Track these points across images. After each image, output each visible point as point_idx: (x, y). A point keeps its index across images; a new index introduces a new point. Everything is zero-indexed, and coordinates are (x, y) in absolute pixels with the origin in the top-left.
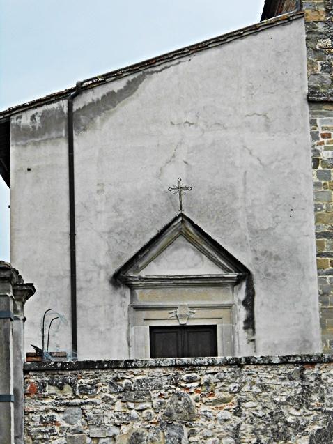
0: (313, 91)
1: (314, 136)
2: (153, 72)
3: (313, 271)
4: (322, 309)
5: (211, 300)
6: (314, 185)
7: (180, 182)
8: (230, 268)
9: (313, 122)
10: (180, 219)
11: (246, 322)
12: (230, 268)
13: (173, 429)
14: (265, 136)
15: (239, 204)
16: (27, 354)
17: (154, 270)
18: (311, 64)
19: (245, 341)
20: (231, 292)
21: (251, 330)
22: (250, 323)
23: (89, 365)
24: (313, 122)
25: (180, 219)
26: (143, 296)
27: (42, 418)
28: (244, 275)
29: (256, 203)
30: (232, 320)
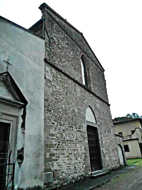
2: (2, 21)
3: (43, 111)
4: (44, 125)
5: (10, 112)
6: (35, 175)
7: (8, 61)
8: (19, 100)
10: (6, 74)
11: (22, 124)
12: (19, 100)
15: (24, 80)
19: (21, 133)
20: (18, 111)
21: (23, 128)
22: (23, 125)
25: (6, 74)
29: (29, 82)
30: (17, 123)
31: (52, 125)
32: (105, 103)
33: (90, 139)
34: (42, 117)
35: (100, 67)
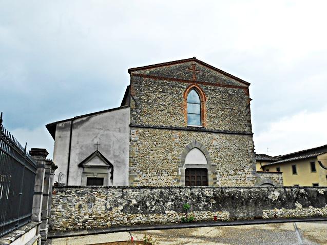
0: (131, 124)
1: (130, 134)
3: (128, 166)
9: (130, 131)
17: (90, 164)
18: (131, 118)
22: (112, 178)
24: (130, 131)
26: (86, 170)
27: (161, 193)
28: (111, 166)
30: (107, 177)
31: (136, 174)
32: (236, 135)
33: (188, 180)
34: (128, 170)
35: (238, 83)
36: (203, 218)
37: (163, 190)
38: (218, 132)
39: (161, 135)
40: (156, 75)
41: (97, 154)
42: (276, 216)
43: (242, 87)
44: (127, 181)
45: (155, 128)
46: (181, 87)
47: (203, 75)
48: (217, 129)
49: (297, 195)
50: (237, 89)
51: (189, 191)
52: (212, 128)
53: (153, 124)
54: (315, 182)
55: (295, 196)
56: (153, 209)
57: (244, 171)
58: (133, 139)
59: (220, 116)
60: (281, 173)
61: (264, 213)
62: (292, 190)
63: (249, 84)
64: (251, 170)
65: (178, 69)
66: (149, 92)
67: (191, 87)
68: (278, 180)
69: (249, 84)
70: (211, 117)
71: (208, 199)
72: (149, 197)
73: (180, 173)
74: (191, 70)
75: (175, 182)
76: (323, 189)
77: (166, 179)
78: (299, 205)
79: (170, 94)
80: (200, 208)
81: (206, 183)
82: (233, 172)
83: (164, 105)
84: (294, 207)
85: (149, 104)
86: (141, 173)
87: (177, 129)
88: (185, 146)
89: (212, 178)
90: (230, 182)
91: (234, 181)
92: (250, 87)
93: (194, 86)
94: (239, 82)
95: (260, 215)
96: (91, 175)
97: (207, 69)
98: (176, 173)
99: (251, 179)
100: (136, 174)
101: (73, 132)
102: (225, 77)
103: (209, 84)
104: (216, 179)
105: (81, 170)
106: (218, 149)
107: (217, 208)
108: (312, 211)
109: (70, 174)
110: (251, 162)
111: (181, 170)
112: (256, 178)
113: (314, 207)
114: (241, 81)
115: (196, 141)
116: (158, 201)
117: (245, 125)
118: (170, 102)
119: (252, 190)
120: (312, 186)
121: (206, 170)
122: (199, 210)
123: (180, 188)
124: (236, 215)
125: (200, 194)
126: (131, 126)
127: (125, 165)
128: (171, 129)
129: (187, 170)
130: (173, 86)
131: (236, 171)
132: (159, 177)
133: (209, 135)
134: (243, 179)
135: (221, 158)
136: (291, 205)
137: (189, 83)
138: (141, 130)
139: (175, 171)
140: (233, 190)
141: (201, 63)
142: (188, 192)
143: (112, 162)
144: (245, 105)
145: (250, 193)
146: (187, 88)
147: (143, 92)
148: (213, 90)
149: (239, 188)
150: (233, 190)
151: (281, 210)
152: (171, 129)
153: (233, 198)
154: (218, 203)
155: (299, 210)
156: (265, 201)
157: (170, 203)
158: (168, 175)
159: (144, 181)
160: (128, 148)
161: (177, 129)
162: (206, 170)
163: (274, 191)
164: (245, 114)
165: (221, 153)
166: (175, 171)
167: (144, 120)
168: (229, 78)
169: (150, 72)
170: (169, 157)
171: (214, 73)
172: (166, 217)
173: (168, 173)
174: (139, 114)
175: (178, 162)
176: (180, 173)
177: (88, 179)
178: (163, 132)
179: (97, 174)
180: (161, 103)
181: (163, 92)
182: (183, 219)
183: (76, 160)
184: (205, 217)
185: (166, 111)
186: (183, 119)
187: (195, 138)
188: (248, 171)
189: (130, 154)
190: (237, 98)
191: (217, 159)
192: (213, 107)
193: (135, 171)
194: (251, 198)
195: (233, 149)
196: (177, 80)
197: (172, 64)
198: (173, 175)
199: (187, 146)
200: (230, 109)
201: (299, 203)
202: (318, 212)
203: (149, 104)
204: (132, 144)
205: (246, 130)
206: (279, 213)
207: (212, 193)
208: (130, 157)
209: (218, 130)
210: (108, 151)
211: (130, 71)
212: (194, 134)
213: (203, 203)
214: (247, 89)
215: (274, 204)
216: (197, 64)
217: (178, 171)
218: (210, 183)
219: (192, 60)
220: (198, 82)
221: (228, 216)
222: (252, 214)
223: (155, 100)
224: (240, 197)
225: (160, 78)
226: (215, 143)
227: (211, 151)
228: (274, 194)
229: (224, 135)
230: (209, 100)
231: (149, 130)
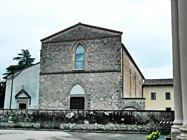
0: (41, 72)
1: (40, 79)
3: (38, 97)
9: (40, 77)
13: (87, 113)
14: (34, 79)
16: (155, 93)
17: (20, 96)
18: (41, 69)
22: (30, 104)
23: (125, 98)
24: (40, 77)
26: (19, 100)
27: (7, 112)
28: (29, 97)
31: (42, 101)
32: (107, 73)
33: (72, 105)
36: (26, 126)
37: (8, 111)
38: (94, 72)
39: (56, 78)
40: (55, 41)
41: (23, 91)
42: (69, 128)
43: (116, 36)
44: (37, 105)
45: (53, 73)
46: (70, 45)
47: (86, 33)
48: (93, 70)
49: (87, 115)
50: (111, 39)
51: (21, 112)
52: (90, 69)
53: (52, 71)
54: (168, 107)
55: (85, 116)
56: (3, 120)
57: (111, 98)
58: (41, 81)
59: (96, 60)
60: (145, 99)
61: (61, 125)
62: (83, 112)
63: (122, 33)
64: (117, 97)
65: (69, 33)
66: (51, 52)
67: (77, 43)
68: (140, 104)
69: (122, 33)
70: (89, 62)
71: (29, 116)
72: (2, 114)
73: (66, 101)
74: (78, 32)
75: (63, 105)
76: (109, 112)
77: (58, 104)
78: (87, 122)
79: (63, 51)
80: (25, 120)
81: (83, 108)
82: (102, 99)
83: (60, 59)
84: (83, 123)
85: (51, 59)
86: (45, 100)
87: (66, 73)
88: (71, 83)
89: (87, 103)
90: (100, 105)
91: (103, 105)
92: (122, 36)
93: (79, 42)
94: (113, 33)
95: (58, 127)
96: (21, 102)
97: (89, 28)
98: (64, 100)
99: (117, 104)
100: (42, 101)
101: (13, 80)
102: (102, 32)
103: (89, 39)
104: (90, 103)
105: (16, 100)
106: (93, 84)
107: (34, 121)
108: (96, 126)
109: (12, 102)
110: (117, 91)
111: (67, 98)
112: (120, 102)
113: (99, 123)
114: (114, 32)
115: (78, 79)
116: (5, 116)
117: (115, 64)
118: (63, 56)
119: (56, 111)
120: (165, 110)
121: (83, 99)
122: (24, 122)
123: (16, 110)
124: (44, 126)
125: (26, 113)
126: (40, 74)
127: (37, 96)
128: (63, 73)
129: (72, 99)
130: (65, 46)
131: (104, 98)
132: (54, 103)
133: (87, 75)
134: (110, 103)
135: (94, 89)
136: (81, 121)
137: (75, 41)
138: (45, 76)
139: (63, 99)
140: (44, 111)
141: (84, 25)
142: (20, 112)
143: (30, 95)
144: (116, 49)
145: (54, 114)
146: (74, 45)
147: (48, 53)
148: (92, 43)
149: (48, 110)
150: (44, 111)
151: (73, 124)
152: (63, 73)
153: (44, 115)
154: (34, 118)
155: (87, 125)
156: (63, 118)
157: (11, 117)
158: (60, 102)
159: (46, 105)
160: (39, 86)
161: (66, 73)
162: (83, 99)
163: (70, 113)
164: (116, 56)
165: (95, 86)
166: (63, 99)
167: (48, 70)
168: (105, 31)
169: (52, 40)
170: (61, 90)
171: (94, 30)
172: (8, 124)
173: (59, 100)
174: (45, 66)
175: (66, 94)
176: (66, 101)
177: (20, 104)
178: (58, 75)
179: (23, 102)
180: (58, 58)
181: (59, 50)
182: (16, 125)
183: (14, 94)
184: (27, 125)
185: (60, 62)
186: (70, 65)
187: (78, 78)
188: (115, 98)
189: (40, 90)
190: (110, 45)
191: (92, 91)
192: (91, 54)
193: (42, 100)
194: (55, 117)
195: (104, 83)
196: (68, 41)
197: (65, 31)
198: (62, 102)
199: (72, 83)
200: (104, 54)
201: (87, 120)
202: (101, 127)
203: (51, 59)
204: (40, 84)
205: (116, 68)
206: (71, 126)
207: (32, 113)
208: (39, 92)
209: (94, 70)
210: (28, 89)
211: (42, 41)
212: (77, 75)
213: (27, 118)
214: (120, 36)
215: (69, 121)
216: (82, 26)
217: (65, 99)
218: (86, 108)
219: (79, 25)
220: (82, 39)
221: (39, 126)
222: (53, 125)
223: (54, 56)
224: (48, 116)
225: (58, 42)
226: (91, 80)
227: (87, 85)
228: (70, 114)
229: (98, 74)
230: (89, 50)
231: (50, 75)
